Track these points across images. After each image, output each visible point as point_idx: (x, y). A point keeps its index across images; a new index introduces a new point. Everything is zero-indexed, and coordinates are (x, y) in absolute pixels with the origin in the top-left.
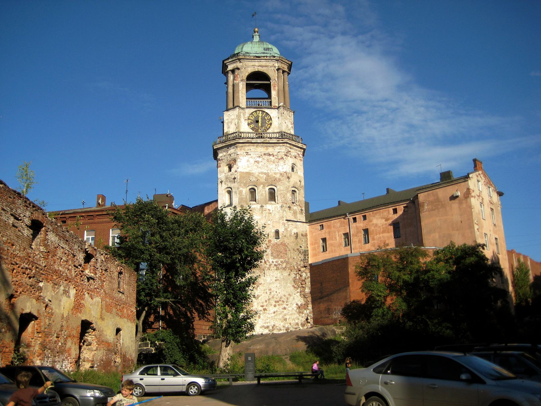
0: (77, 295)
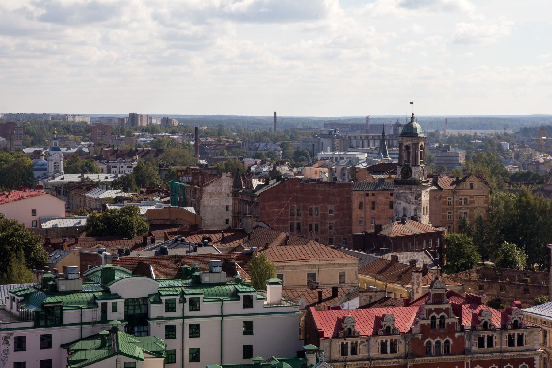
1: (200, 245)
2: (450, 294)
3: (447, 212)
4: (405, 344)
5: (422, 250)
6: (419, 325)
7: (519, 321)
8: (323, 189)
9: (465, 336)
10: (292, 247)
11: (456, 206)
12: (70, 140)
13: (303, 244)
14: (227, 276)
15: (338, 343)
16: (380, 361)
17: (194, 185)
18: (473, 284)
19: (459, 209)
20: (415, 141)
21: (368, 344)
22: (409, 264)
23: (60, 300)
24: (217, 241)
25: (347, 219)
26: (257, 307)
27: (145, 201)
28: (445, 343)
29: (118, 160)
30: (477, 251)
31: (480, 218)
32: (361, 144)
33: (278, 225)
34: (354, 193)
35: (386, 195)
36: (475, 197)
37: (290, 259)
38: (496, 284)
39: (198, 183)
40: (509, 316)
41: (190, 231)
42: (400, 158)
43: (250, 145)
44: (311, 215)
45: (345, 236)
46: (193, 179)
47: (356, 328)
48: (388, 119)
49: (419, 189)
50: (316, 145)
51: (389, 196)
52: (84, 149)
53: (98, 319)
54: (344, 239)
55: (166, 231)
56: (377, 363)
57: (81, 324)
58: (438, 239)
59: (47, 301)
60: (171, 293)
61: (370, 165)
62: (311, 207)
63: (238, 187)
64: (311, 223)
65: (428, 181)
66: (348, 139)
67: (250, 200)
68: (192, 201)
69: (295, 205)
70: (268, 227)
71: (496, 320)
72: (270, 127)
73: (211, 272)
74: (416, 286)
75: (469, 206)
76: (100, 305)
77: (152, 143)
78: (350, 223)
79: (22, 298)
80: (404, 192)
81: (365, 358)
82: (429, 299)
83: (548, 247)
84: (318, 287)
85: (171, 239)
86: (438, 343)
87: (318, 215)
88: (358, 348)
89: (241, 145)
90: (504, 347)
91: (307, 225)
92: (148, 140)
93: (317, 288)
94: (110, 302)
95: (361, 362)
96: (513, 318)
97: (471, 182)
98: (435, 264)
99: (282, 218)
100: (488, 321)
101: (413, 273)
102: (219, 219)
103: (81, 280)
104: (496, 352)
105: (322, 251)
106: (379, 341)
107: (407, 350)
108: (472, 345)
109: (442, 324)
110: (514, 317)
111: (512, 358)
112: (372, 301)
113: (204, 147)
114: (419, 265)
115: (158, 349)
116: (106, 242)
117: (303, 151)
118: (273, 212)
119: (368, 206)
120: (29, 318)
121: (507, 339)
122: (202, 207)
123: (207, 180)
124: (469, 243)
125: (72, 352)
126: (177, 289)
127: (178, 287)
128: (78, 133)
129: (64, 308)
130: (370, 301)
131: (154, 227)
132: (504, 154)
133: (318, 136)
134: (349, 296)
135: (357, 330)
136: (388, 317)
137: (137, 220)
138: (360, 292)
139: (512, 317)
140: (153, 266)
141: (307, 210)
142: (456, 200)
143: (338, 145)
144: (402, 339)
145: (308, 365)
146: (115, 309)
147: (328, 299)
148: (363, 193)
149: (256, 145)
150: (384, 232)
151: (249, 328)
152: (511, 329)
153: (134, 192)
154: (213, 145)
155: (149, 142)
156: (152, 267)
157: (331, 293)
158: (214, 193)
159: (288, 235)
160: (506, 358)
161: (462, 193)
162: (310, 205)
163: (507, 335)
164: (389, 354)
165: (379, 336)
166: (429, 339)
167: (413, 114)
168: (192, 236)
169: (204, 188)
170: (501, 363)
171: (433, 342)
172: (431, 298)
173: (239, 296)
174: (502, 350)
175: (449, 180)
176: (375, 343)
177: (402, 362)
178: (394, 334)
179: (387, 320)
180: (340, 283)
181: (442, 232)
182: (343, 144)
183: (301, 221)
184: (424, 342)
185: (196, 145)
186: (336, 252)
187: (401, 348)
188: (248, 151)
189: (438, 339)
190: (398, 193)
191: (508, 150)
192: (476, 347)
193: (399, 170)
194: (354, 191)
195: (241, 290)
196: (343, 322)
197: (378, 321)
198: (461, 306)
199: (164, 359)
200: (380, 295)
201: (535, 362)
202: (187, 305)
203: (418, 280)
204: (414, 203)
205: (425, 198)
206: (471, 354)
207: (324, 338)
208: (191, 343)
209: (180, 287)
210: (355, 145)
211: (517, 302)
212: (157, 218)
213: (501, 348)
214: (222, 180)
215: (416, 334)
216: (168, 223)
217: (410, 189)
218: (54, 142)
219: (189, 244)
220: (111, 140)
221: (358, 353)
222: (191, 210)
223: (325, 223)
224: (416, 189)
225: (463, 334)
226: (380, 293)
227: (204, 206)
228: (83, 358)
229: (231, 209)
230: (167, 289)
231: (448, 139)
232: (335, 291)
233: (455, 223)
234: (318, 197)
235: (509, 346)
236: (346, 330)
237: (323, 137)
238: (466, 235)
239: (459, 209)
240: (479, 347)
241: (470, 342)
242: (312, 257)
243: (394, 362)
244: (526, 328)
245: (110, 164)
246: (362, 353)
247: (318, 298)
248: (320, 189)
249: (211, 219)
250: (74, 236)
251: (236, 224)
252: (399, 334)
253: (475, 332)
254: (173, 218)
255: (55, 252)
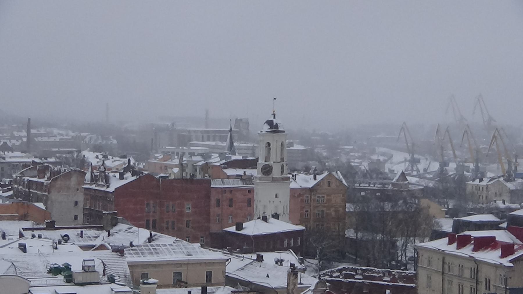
1: (60, 243)
36: (332, 196)
222: (41, 205)
229: (81, 205)
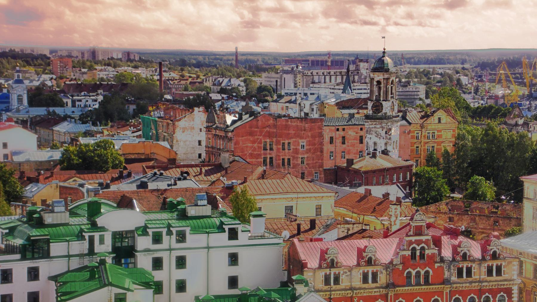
0: (221, 128)
1: (179, 179)
2: (429, 226)
3: (415, 146)
4: (386, 274)
5: (393, 184)
6: (399, 255)
7: (498, 252)
8: (295, 124)
9: (445, 266)
10: (270, 181)
11: (423, 140)
12: (30, 73)
13: (280, 178)
14: (212, 209)
15: (321, 274)
16: (362, 291)
17: (166, 119)
18: (443, 216)
19: (426, 143)
20: (386, 76)
21: (351, 274)
22: (382, 197)
23: (47, 233)
24: (195, 175)
25: (319, 153)
26: (243, 238)
27: (117, 135)
28: (425, 273)
29: (83, 94)
30: (446, 184)
31: (446, 152)
32: (323, 81)
33: (252, 160)
34: (325, 128)
35: (356, 130)
37: (268, 192)
38: (466, 216)
39: (170, 117)
40: (488, 247)
41: (168, 165)
42: (372, 92)
43: (213, 80)
44: (284, 149)
45: (317, 170)
46: (165, 114)
47: (339, 260)
48: (397, 54)
49: (389, 124)
50: (279, 80)
51: (359, 131)
52: (46, 82)
53: (86, 252)
54: (316, 173)
55: (144, 164)
56: (359, 293)
57: (69, 256)
58: (408, 173)
59: (34, 234)
60: (157, 226)
61: (339, 101)
62: (284, 141)
63: (212, 122)
64: (283, 157)
65: (398, 116)
66: (310, 74)
67: (224, 135)
68: (164, 136)
69: (268, 140)
70: (244, 161)
71: (476, 251)
72: (230, 62)
73: (197, 205)
74: (393, 219)
75: (436, 140)
76: (87, 238)
77: (116, 77)
78: (321, 157)
79: (7, 231)
80: (375, 127)
81: (348, 288)
82: (410, 231)
83: (521, 179)
84: (296, 219)
85: (150, 173)
86: (418, 273)
87: (290, 150)
88: (341, 278)
89: (205, 80)
90: (482, 277)
91: (280, 160)
92: (111, 74)
93: (296, 220)
94: (97, 235)
95: (343, 292)
96: (491, 249)
97: (439, 117)
98: (406, 197)
99: (255, 153)
100: (467, 252)
101: (390, 206)
102: (191, 154)
103: (68, 213)
104: (475, 282)
105: (299, 185)
106: (361, 271)
107: (388, 280)
108: (451, 275)
109: (422, 256)
110: (492, 248)
111: (490, 287)
112: (350, 233)
113: (168, 82)
114: (393, 198)
115: (147, 281)
116: (82, 176)
117: (266, 86)
118: (247, 147)
119: (338, 141)
120: (15, 250)
121: (486, 270)
122: (175, 142)
123: (179, 115)
124: (438, 176)
125: (61, 283)
126: (163, 222)
127: (164, 220)
128: (38, 65)
129: (51, 241)
130: (348, 233)
131: (129, 161)
132: (463, 88)
133: (280, 72)
134: (328, 228)
135: (340, 261)
136: (370, 249)
137: (112, 154)
138: (338, 224)
139: (491, 248)
140: (135, 199)
141: (280, 145)
142: (423, 134)
143: (300, 81)
144: (384, 269)
145: (297, 295)
146: (102, 241)
147: (306, 231)
148: (333, 128)
149: (219, 81)
150: (356, 166)
151: (234, 259)
152: (489, 260)
153: (103, 126)
154: (176, 80)
155: (112, 76)
156: (135, 201)
157: (309, 226)
158: (186, 128)
159: (265, 169)
160: (485, 288)
161: (429, 127)
162: (283, 140)
163: (486, 265)
164: (371, 284)
165: (361, 266)
166: (410, 270)
167: (384, 49)
168: (170, 170)
169: (176, 123)
170: (480, 292)
171: (414, 273)
172: (412, 230)
173: (224, 229)
174: (481, 280)
175: (417, 115)
176: (358, 275)
177: (383, 291)
178: (375, 265)
179: (368, 251)
180: (317, 215)
181: (411, 166)
182: (305, 80)
183: (273, 156)
184: (404, 273)
185: (160, 80)
186: (312, 186)
187: (383, 279)
188: (212, 87)
189: (418, 269)
190: (369, 128)
191: (466, 85)
192: (455, 277)
193: (370, 104)
194: (325, 126)
195: (226, 223)
196: (326, 253)
197: (360, 252)
198: (440, 238)
199: (153, 290)
200: (357, 227)
201: (513, 292)
202: (174, 237)
203: (396, 212)
204: (385, 137)
205: (395, 131)
206: (451, 284)
207: (308, 268)
208: (179, 274)
209: (167, 220)
210: (317, 81)
211: (496, 233)
212: (132, 153)
213: (480, 278)
214: (194, 115)
215: (396, 265)
216: (143, 157)
217: (381, 124)
218: (16, 74)
219: (170, 178)
220: (72, 74)
221: (341, 283)
222: (165, 144)
223: (297, 158)
224: (387, 124)
225: (442, 264)
226: (357, 225)
227: (177, 141)
228: (73, 290)
229: (204, 144)
230: (154, 222)
231: (407, 74)
232: (313, 224)
233: (422, 157)
234: (290, 132)
235: (488, 276)
236: (329, 260)
237: (285, 73)
238: (435, 168)
239: (426, 143)
240: (458, 278)
241: (449, 273)
242: (289, 190)
243: (375, 292)
244: (505, 259)
245: (74, 98)
246: (345, 282)
247: (296, 230)
248: (293, 124)
249: (184, 154)
250: (47, 170)
251: (210, 160)
252: (381, 265)
253: (454, 263)
254: (148, 152)
255: (31, 185)
